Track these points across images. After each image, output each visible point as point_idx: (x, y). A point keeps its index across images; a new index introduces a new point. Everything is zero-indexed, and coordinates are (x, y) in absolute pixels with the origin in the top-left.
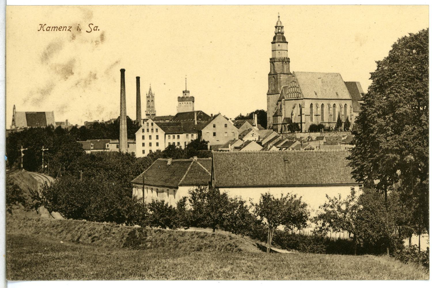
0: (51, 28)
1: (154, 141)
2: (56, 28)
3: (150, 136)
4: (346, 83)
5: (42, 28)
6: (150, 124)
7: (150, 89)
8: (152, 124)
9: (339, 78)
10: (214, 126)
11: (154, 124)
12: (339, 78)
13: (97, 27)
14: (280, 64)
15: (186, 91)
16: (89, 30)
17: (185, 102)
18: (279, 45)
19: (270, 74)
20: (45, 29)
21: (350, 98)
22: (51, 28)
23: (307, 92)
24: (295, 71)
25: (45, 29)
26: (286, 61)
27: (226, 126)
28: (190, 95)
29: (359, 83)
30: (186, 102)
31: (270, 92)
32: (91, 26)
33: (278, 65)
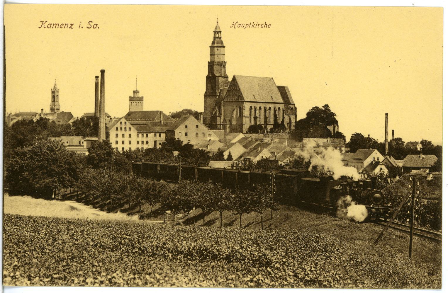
0: (64, 25)
1: (127, 139)
2: (58, 25)
3: (123, 135)
4: (277, 86)
5: (43, 25)
6: (123, 123)
7: (55, 84)
8: (126, 123)
9: (272, 82)
10: (186, 127)
11: (127, 123)
12: (272, 82)
13: (97, 25)
14: (218, 67)
15: (136, 90)
16: (89, 26)
17: (136, 101)
18: (218, 49)
19: (208, 78)
20: (46, 26)
21: (283, 102)
22: (52, 25)
23: (247, 95)
24: (237, 73)
25: (46, 26)
26: (223, 65)
27: (197, 126)
28: (140, 95)
29: (287, 87)
30: (137, 102)
31: (208, 94)
32: (90, 23)
33: (216, 68)
